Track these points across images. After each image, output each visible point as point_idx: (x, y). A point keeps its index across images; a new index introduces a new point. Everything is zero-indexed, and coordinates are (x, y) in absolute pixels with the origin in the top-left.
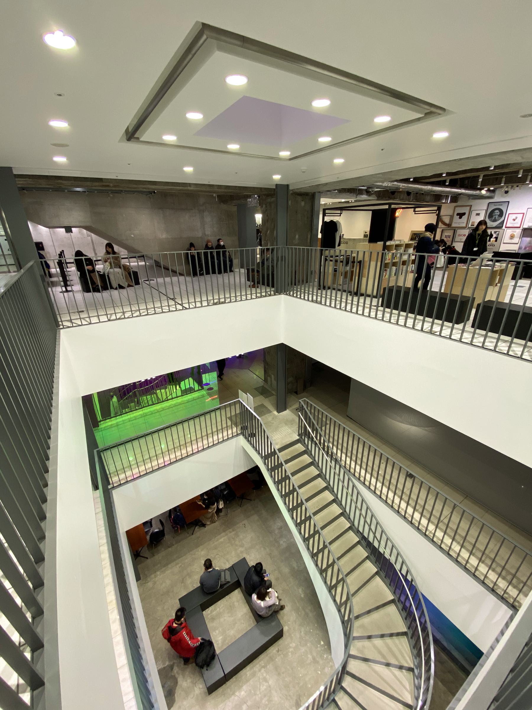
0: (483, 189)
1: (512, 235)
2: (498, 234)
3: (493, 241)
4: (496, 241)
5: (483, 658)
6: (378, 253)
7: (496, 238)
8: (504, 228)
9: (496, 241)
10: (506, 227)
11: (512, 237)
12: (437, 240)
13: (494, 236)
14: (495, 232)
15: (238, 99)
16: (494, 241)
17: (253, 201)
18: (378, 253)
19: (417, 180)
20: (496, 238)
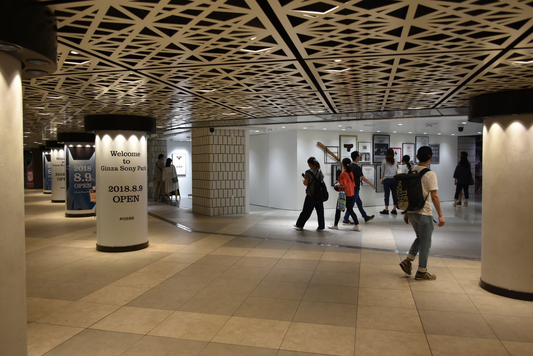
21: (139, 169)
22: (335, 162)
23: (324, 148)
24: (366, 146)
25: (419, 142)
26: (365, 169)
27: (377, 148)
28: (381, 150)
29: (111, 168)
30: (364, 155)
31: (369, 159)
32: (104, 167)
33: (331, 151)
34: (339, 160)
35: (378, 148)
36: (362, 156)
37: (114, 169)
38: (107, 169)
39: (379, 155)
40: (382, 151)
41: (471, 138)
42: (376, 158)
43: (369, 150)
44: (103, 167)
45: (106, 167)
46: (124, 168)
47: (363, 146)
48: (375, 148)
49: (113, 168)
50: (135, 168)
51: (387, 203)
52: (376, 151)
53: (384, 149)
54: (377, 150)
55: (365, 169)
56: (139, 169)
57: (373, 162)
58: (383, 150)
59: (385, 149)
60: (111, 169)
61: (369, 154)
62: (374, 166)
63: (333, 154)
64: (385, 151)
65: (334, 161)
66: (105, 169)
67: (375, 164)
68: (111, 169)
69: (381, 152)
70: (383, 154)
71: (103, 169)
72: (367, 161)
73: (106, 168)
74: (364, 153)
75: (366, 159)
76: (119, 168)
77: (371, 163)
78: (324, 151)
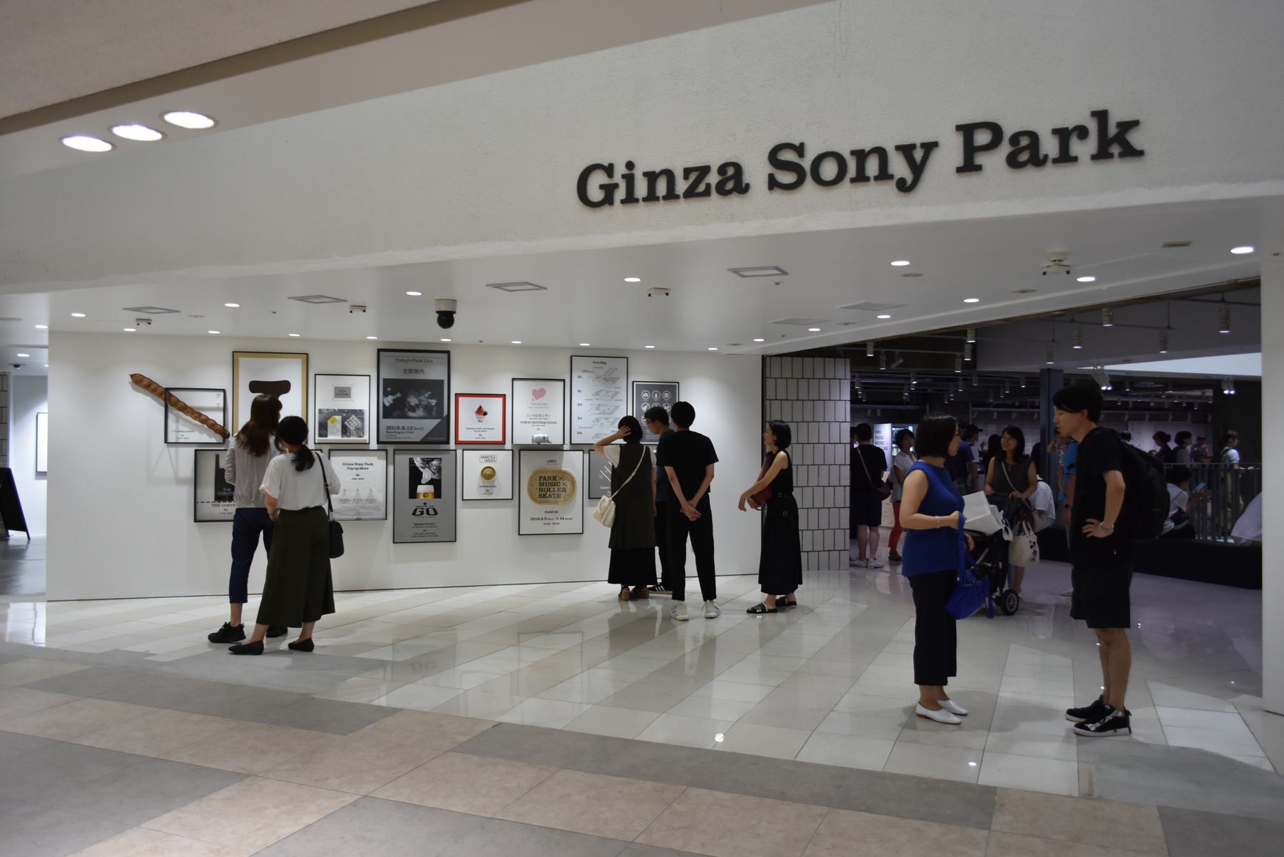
0: (1191, 449)
1: (488, 472)
2: (439, 470)
3: (425, 495)
4: (437, 494)
5: (1011, 546)
6: (545, 524)
7: (436, 483)
8: (452, 445)
9: (437, 494)
10: (457, 442)
11: (488, 475)
12: (945, 463)
13: (427, 475)
14: (427, 462)
15: (1130, 686)
16: (430, 497)
17: (1256, 466)
18: (545, 524)
19: (937, 334)
20: (436, 483)
21: (980, 159)
22: (214, 440)
23: (160, 395)
24: (349, 389)
25: (585, 376)
26: (344, 464)
27: (392, 393)
28: (413, 401)
29: (679, 175)
30: (339, 418)
31: (360, 431)
32: (609, 170)
33: (188, 404)
34: (224, 434)
35: (399, 395)
36: (329, 422)
37: (713, 178)
38: (641, 189)
39: (404, 416)
40: (417, 406)
41: (808, 360)
42: (389, 428)
43: (364, 397)
44: (598, 179)
45: (638, 173)
46: (806, 163)
47: (336, 388)
48: (386, 395)
49: (704, 170)
50: (918, 155)
51: (238, 594)
52: (387, 404)
53: (422, 398)
54: (393, 400)
55: (344, 464)
56: (980, 159)
57: (379, 442)
58: (419, 401)
59: (431, 397)
60: (681, 186)
61: (359, 413)
62: (384, 453)
63: (201, 414)
64: (430, 403)
65: (210, 437)
66: (620, 194)
67: (391, 448)
68: (681, 186)
69: (413, 409)
70: (420, 412)
71: (595, 194)
72: (353, 439)
73: (629, 179)
74: (340, 412)
75: (345, 431)
76: (757, 171)
77: (374, 445)
78: (163, 403)
